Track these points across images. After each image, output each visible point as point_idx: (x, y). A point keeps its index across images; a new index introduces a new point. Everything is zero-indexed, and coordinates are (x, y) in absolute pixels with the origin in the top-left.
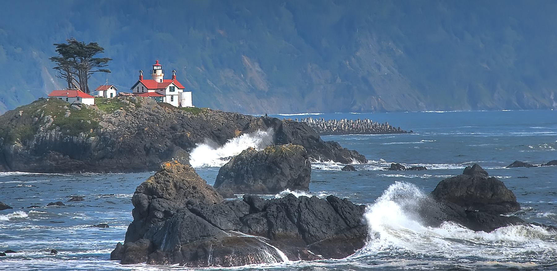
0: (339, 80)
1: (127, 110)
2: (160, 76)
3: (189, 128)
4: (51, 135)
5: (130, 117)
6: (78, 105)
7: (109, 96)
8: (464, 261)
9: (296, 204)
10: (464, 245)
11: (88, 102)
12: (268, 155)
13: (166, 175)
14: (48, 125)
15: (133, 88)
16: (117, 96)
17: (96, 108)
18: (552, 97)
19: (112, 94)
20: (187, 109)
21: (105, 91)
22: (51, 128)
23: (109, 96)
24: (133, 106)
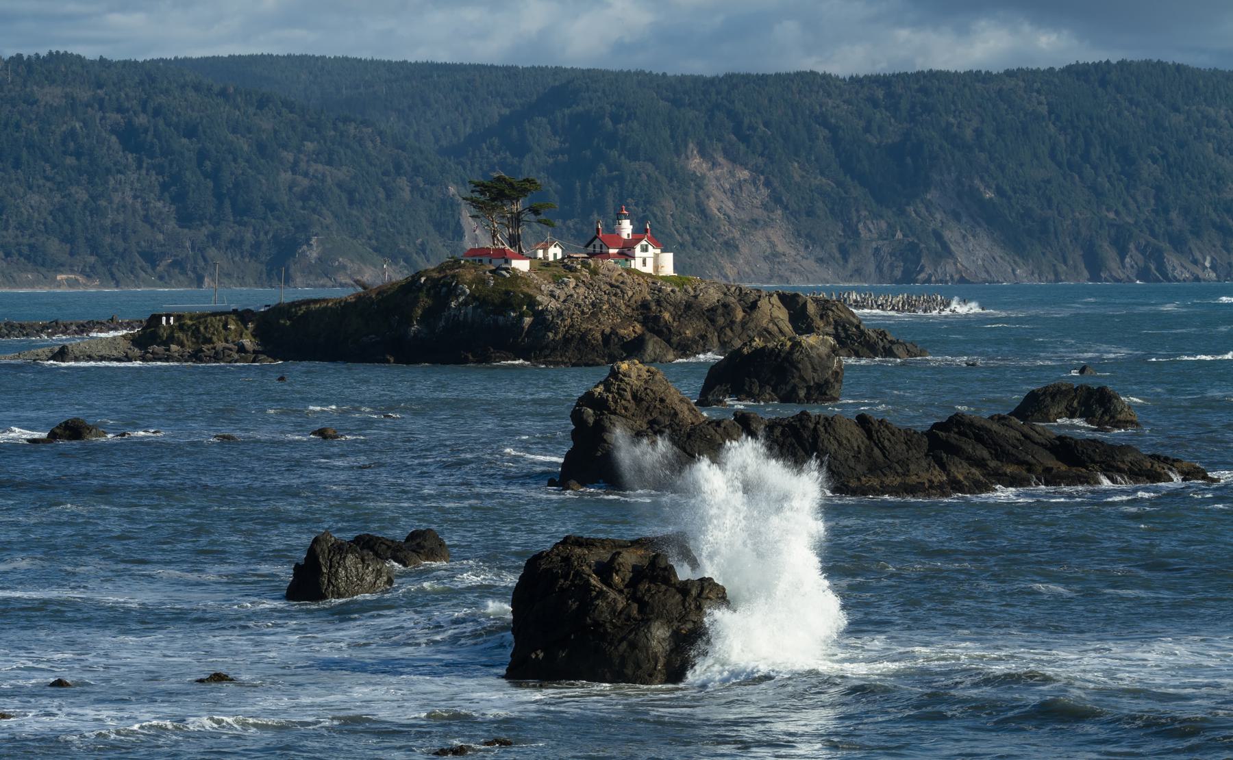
0: (899, 235)
1: (577, 278)
2: (626, 228)
3: (669, 307)
4: (466, 314)
5: (582, 290)
7: (551, 259)
9: (811, 426)
11: (522, 265)
12: (780, 351)
13: (622, 380)
15: (587, 246)
16: (563, 258)
18: (1207, 264)
19: (555, 255)
20: (666, 279)
21: (545, 249)
22: (465, 303)
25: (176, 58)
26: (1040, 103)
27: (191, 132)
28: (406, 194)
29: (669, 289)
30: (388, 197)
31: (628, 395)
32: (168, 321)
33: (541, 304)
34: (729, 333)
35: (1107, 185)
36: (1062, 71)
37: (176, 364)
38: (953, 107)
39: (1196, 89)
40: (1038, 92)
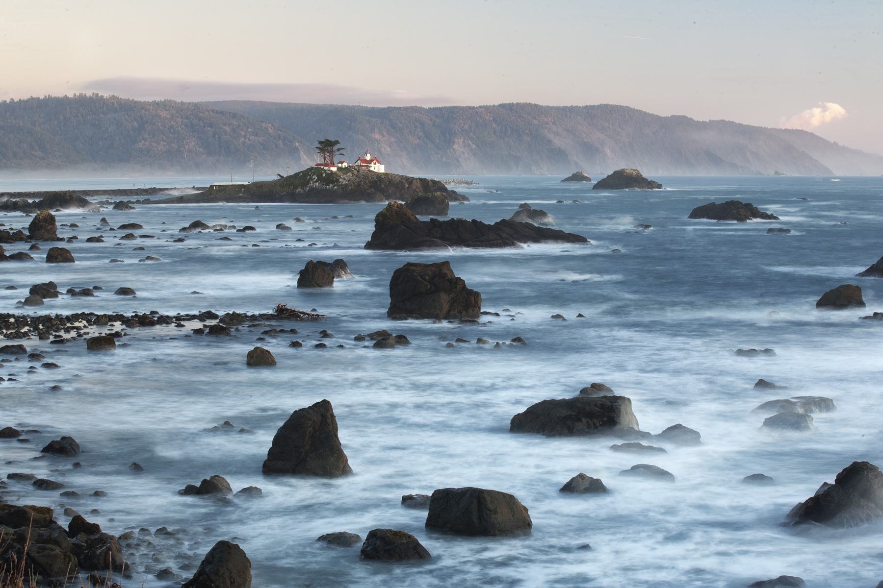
1: (353, 174)
4: (316, 186)
5: (354, 177)
6: (329, 170)
8: (578, 224)
10: (662, 532)
14: (314, 180)
15: (355, 163)
17: (338, 172)
18: (545, 169)
23: (344, 167)
24: (356, 172)
25: (133, 100)
26: (490, 116)
27: (211, 125)
28: (282, 146)
29: (383, 177)
30: (276, 147)
31: (394, 212)
32: (216, 187)
33: (340, 182)
34: (403, 191)
35: (513, 143)
36: (498, 106)
37: (580, 195)
38: (462, 118)
39: (541, 112)
40: (490, 113)
